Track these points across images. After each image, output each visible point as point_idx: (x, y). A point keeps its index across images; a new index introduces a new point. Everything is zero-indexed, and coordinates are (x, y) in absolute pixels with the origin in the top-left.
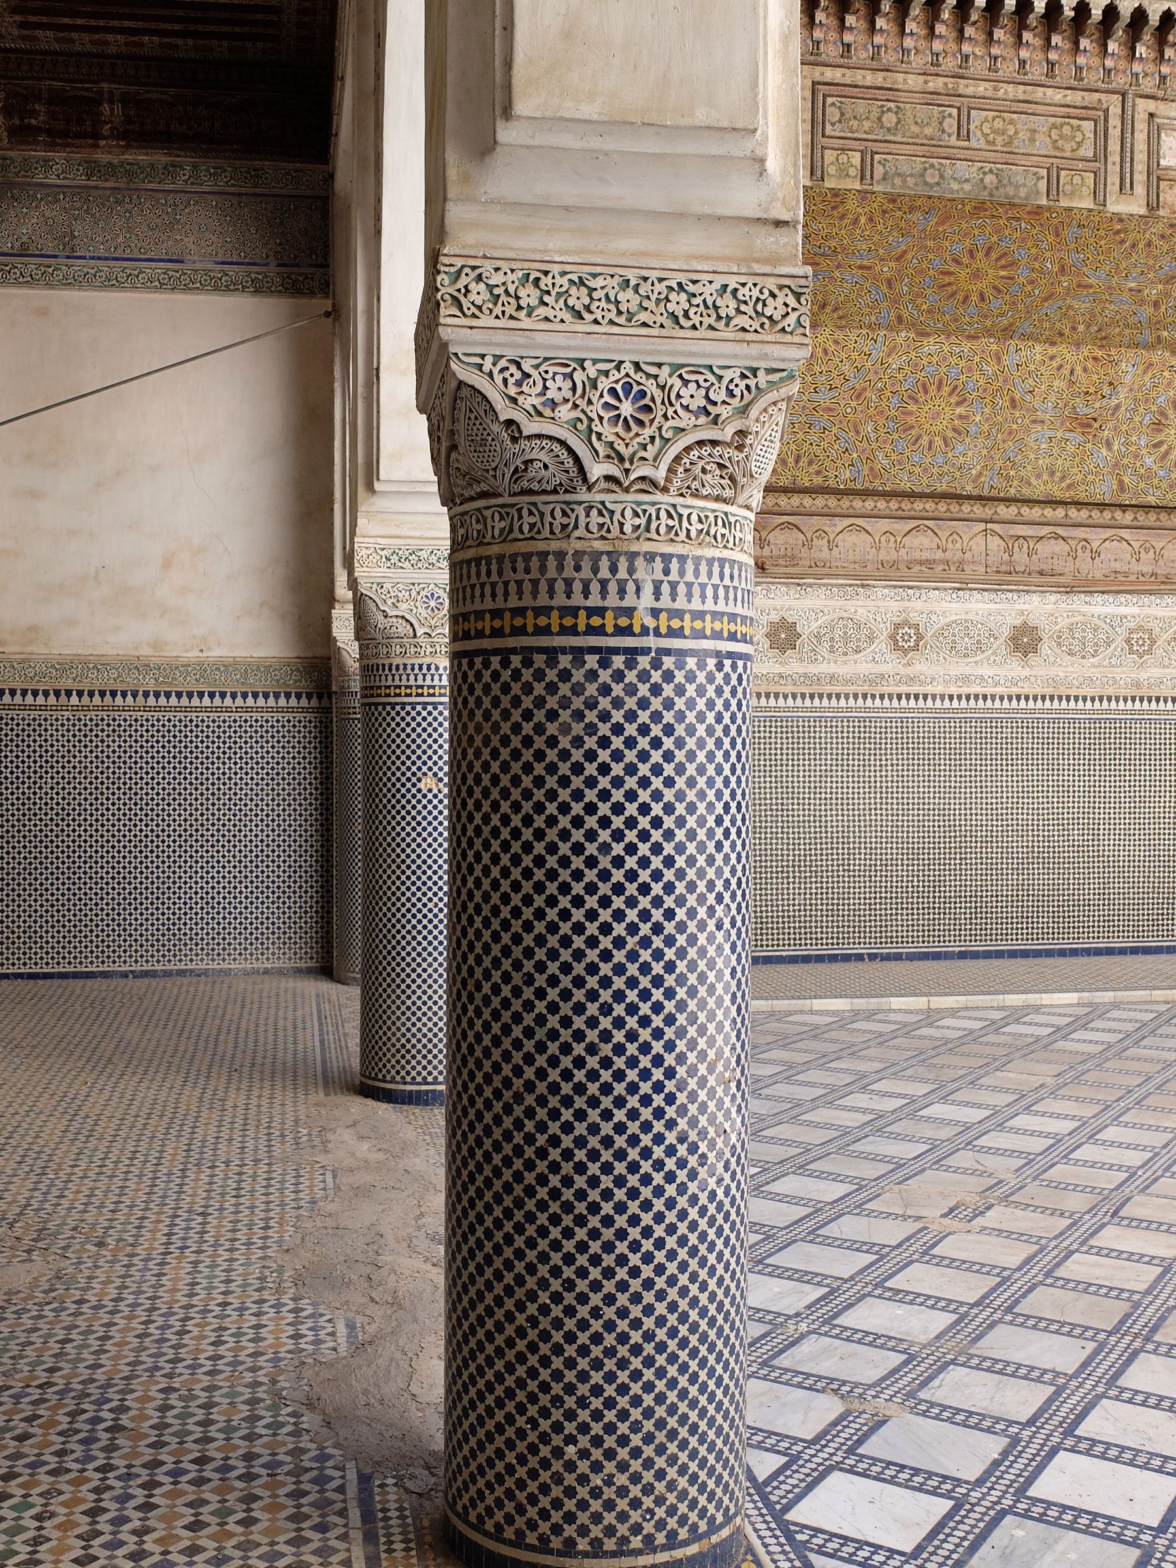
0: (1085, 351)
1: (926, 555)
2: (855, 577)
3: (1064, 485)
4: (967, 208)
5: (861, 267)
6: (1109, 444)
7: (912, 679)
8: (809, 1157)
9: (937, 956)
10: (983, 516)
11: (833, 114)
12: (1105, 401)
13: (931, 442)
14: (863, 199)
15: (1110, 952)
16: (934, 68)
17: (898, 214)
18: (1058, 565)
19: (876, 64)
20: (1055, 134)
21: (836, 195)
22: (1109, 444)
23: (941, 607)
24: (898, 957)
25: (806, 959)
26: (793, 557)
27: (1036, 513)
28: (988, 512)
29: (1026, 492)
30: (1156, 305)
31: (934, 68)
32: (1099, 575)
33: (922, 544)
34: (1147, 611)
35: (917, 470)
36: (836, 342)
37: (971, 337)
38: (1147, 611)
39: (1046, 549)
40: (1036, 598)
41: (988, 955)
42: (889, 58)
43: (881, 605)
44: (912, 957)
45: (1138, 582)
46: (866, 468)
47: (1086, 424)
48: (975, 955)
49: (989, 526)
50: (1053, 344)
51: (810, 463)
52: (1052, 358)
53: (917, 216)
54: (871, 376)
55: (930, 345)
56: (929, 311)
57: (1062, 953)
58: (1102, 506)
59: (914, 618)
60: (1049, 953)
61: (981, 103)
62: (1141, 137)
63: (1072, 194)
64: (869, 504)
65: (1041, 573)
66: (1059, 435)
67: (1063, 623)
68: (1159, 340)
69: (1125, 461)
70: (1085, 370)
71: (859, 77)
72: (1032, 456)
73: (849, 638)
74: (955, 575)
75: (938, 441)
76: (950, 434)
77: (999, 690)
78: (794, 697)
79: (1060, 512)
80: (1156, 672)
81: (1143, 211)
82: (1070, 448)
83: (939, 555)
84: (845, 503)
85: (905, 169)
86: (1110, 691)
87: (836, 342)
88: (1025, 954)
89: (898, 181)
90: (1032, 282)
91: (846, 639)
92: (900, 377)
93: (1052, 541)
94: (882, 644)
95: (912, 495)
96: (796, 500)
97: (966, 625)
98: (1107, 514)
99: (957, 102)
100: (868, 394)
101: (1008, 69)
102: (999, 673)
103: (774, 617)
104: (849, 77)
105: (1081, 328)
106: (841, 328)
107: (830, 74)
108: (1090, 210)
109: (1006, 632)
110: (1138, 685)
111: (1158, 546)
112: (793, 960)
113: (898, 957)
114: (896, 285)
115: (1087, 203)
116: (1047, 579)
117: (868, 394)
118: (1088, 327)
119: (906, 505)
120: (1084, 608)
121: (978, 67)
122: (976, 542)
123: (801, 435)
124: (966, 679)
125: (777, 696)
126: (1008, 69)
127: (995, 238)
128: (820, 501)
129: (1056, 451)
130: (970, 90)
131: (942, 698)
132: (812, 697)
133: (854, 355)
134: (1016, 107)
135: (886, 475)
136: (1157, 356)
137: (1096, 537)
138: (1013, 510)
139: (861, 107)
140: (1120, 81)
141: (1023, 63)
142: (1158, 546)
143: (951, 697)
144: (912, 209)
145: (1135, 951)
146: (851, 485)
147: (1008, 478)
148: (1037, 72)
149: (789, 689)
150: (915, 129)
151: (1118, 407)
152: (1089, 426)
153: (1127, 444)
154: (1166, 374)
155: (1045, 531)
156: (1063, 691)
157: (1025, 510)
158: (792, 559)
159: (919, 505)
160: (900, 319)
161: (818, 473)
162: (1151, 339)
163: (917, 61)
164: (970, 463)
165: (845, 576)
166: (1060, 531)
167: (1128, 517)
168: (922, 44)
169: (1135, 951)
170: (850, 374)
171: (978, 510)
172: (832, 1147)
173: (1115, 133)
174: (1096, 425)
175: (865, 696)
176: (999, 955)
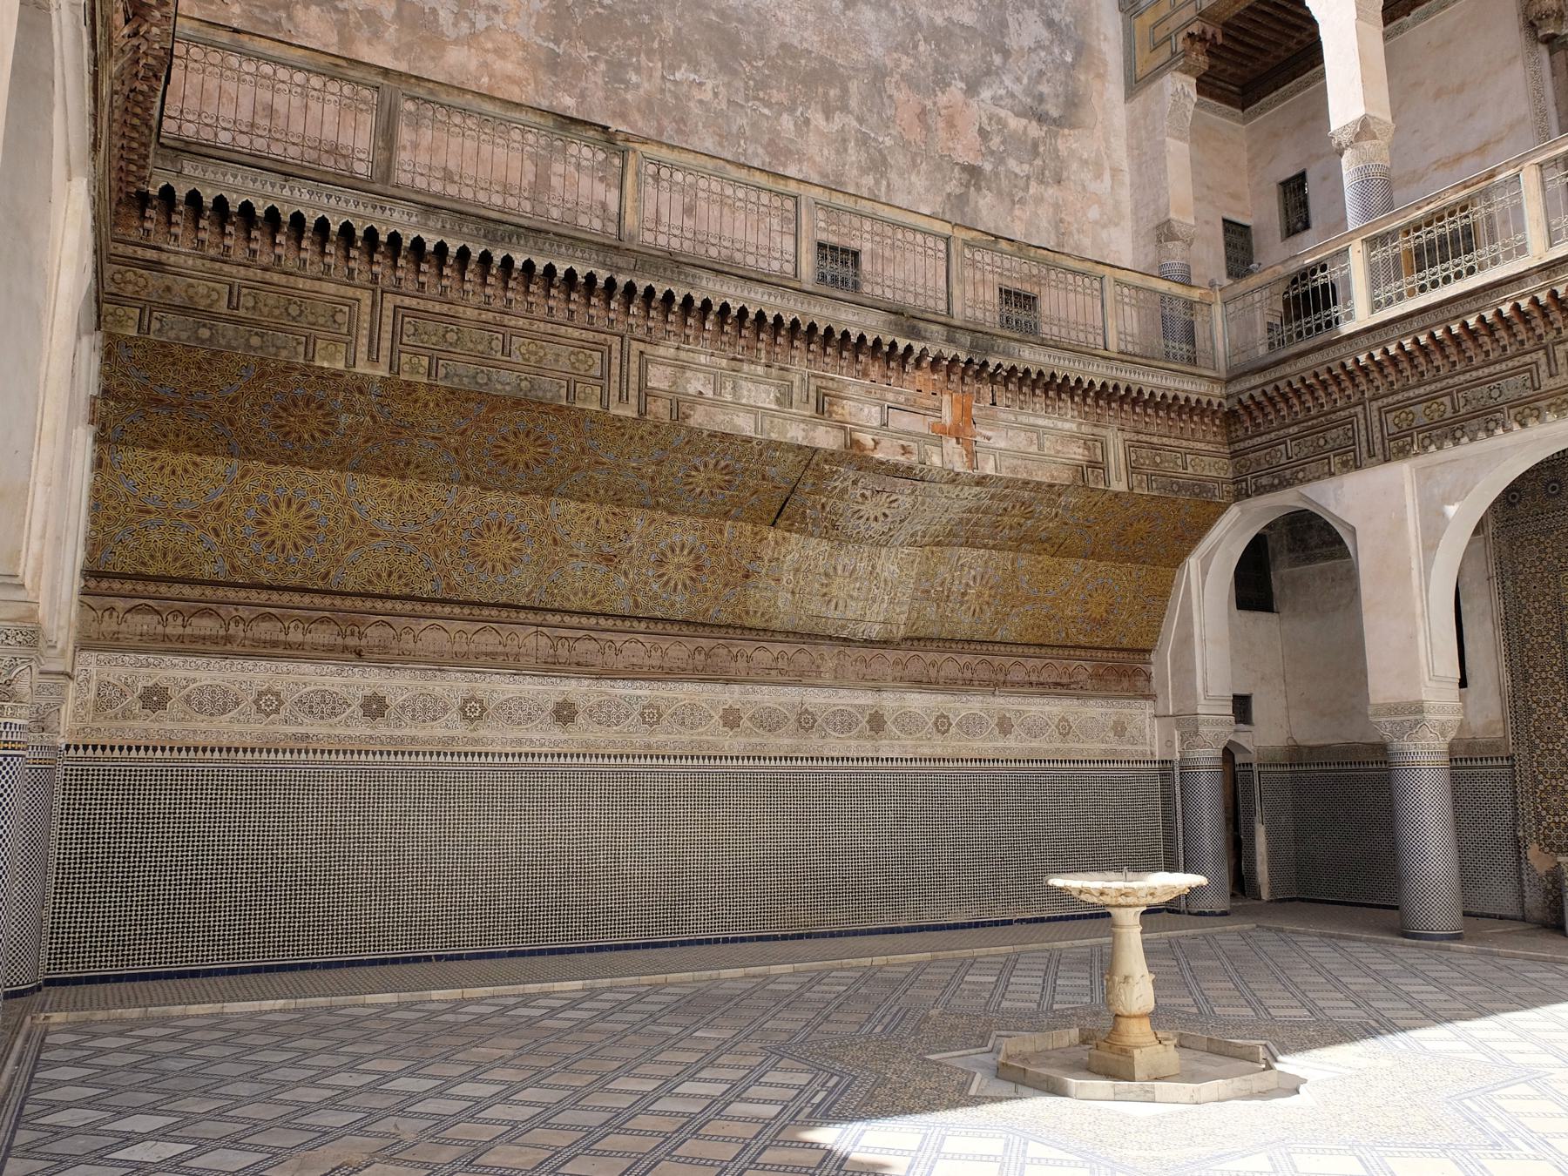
0: (607, 508)
1: (490, 649)
2: (435, 663)
6: (626, 574)
7: (476, 741)
8: (443, 1125)
9: (491, 956)
11: (409, 329)
15: (627, 947)
16: (486, 306)
18: (590, 659)
19: (443, 297)
20: (573, 358)
22: (626, 574)
23: (501, 687)
24: (459, 957)
25: (384, 962)
26: (385, 647)
27: (575, 620)
28: (539, 619)
29: (567, 605)
31: (486, 306)
32: (621, 666)
33: (488, 641)
34: (656, 693)
38: (656, 693)
39: (581, 647)
40: (573, 682)
41: (532, 953)
42: (451, 295)
43: (453, 685)
44: (470, 957)
45: (649, 672)
47: (609, 559)
48: (522, 954)
50: (153, 449)
51: (400, 577)
53: (472, 405)
55: (491, 497)
56: (489, 473)
57: (590, 950)
58: (623, 617)
59: (479, 694)
60: (580, 950)
61: (519, 332)
62: (634, 366)
63: (585, 400)
64: (447, 609)
65: (578, 664)
67: (594, 700)
68: (658, 504)
71: (430, 306)
73: (429, 709)
74: (512, 664)
77: (545, 750)
78: (381, 753)
79: (593, 621)
80: (662, 737)
81: (635, 415)
83: (500, 649)
84: (428, 608)
85: (460, 372)
86: (628, 751)
88: (561, 951)
89: (456, 380)
91: (425, 710)
94: (454, 715)
95: (480, 604)
96: (389, 605)
97: (520, 701)
98: (627, 623)
99: (502, 330)
101: (540, 312)
102: (545, 737)
103: (368, 692)
104: (422, 305)
107: (407, 302)
109: (551, 706)
110: (649, 746)
111: (664, 647)
112: (372, 963)
113: (459, 957)
115: (595, 407)
116: (581, 668)
119: (476, 611)
120: (610, 690)
121: (517, 308)
122: (529, 640)
123: (167, 536)
124: (519, 742)
125: (367, 753)
126: (540, 312)
128: (408, 606)
129: (588, 577)
130: (512, 323)
131: (500, 755)
132: (396, 754)
133: (434, 501)
134: (545, 337)
136: (658, 514)
137: (619, 639)
138: (558, 618)
139: (431, 326)
140: (619, 328)
141: (551, 309)
142: (664, 647)
143: (507, 755)
144: (467, 400)
145: (646, 946)
146: (432, 595)
147: (552, 594)
148: (560, 316)
149: (378, 748)
150: (471, 345)
151: (631, 548)
153: (638, 574)
155: (581, 633)
156: (593, 751)
157: (567, 619)
158: (384, 648)
159: (486, 612)
160: (467, 477)
161: (406, 585)
162: (652, 502)
163: (473, 300)
164: (524, 582)
165: (426, 663)
166: (593, 634)
167: (643, 625)
168: (478, 289)
169: (646, 946)
170: (431, 514)
171: (531, 617)
172: (636, 1109)
173: (616, 362)
175: (438, 754)
176: (541, 952)
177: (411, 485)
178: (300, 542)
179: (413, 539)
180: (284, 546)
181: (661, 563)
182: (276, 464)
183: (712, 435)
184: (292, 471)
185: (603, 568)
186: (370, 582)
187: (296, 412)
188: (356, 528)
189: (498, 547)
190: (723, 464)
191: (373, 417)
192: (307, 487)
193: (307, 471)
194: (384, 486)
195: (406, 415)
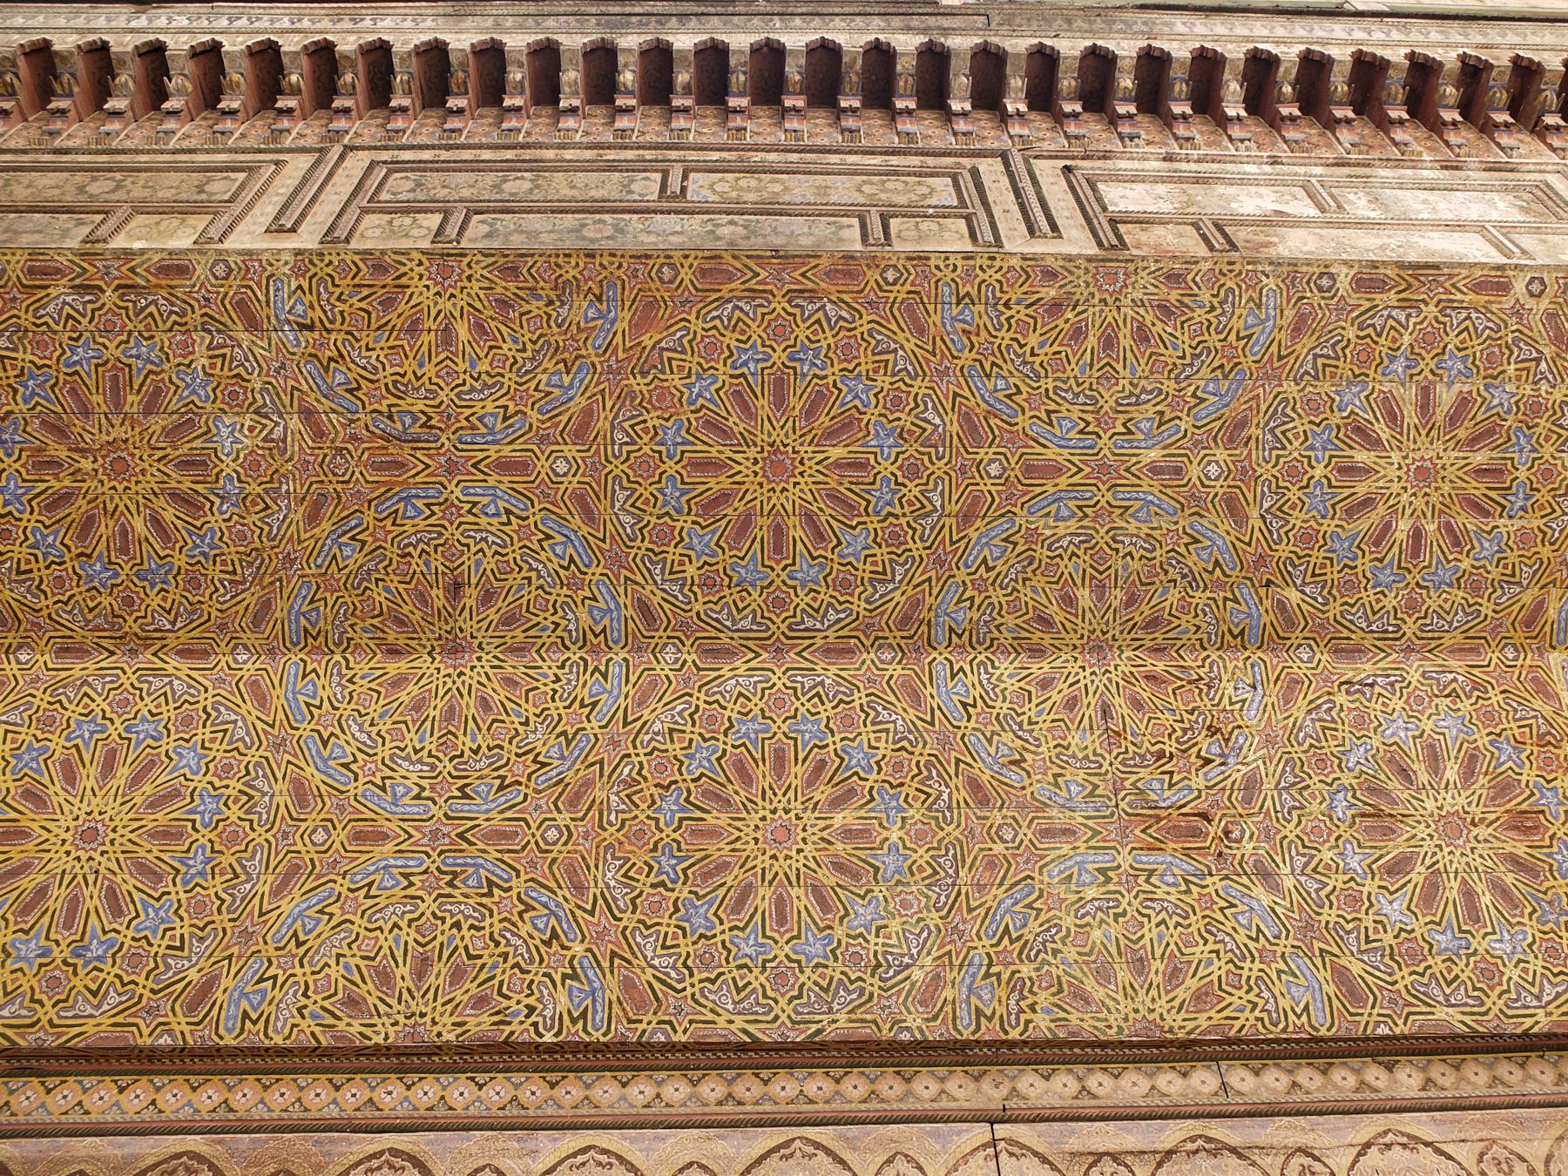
3: (1181, 994)
4: (686, 274)
5: (504, 466)
6: (1266, 875)
10: (978, 1103)
12: (1214, 771)
13: (781, 903)
14: (445, 272)
17: (536, 307)
21: (380, 268)
27: (1132, 1086)
28: (990, 1091)
29: (1083, 1023)
30: (1233, 507)
35: (757, 979)
36: (510, 682)
37: (830, 652)
46: (612, 982)
47: (1188, 828)
49: (1002, 1130)
50: (1037, 652)
51: (457, 976)
52: (1045, 684)
53: (579, 310)
54: (603, 752)
55: (737, 675)
56: (708, 584)
64: (640, 1091)
66: (1124, 859)
69: (1329, 915)
70: (1137, 704)
72: (1068, 921)
75: (800, 898)
76: (828, 878)
82: (1167, 893)
87: (510, 682)
90: (913, 472)
92: (676, 748)
93: (1203, 1161)
96: (427, 1092)
100: (599, 793)
105: (1084, 596)
106: (518, 650)
108: (968, 256)
114: (602, 508)
117: (599, 793)
118: (1100, 590)
123: (429, 905)
127: (779, 356)
128: (497, 1092)
135: (672, 999)
136: (1301, 663)
144: (563, 290)
147: (1018, 986)
151: (1251, 785)
152: (1196, 833)
154: (1341, 698)
155: (1172, 1133)
159: (785, 1088)
161: (480, 1002)
164: (902, 954)
166: (1219, 1130)
171: (961, 1089)
174: (1213, 830)
177: (479, 669)
178: (127, 882)
179: (498, 835)
180: (74, 903)
181: (1378, 818)
182: (81, 652)
183: (1370, 279)
184: (128, 668)
185: (1171, 862)
186: (353, 1003)
187: (94, 435)
188: (313, 818)
189: (786, 833)
190: (1446, 397)
191: (308, 414)
192: (169, 712)
193: (173, 663)
194: (399, 682)
195: (398, 389)
